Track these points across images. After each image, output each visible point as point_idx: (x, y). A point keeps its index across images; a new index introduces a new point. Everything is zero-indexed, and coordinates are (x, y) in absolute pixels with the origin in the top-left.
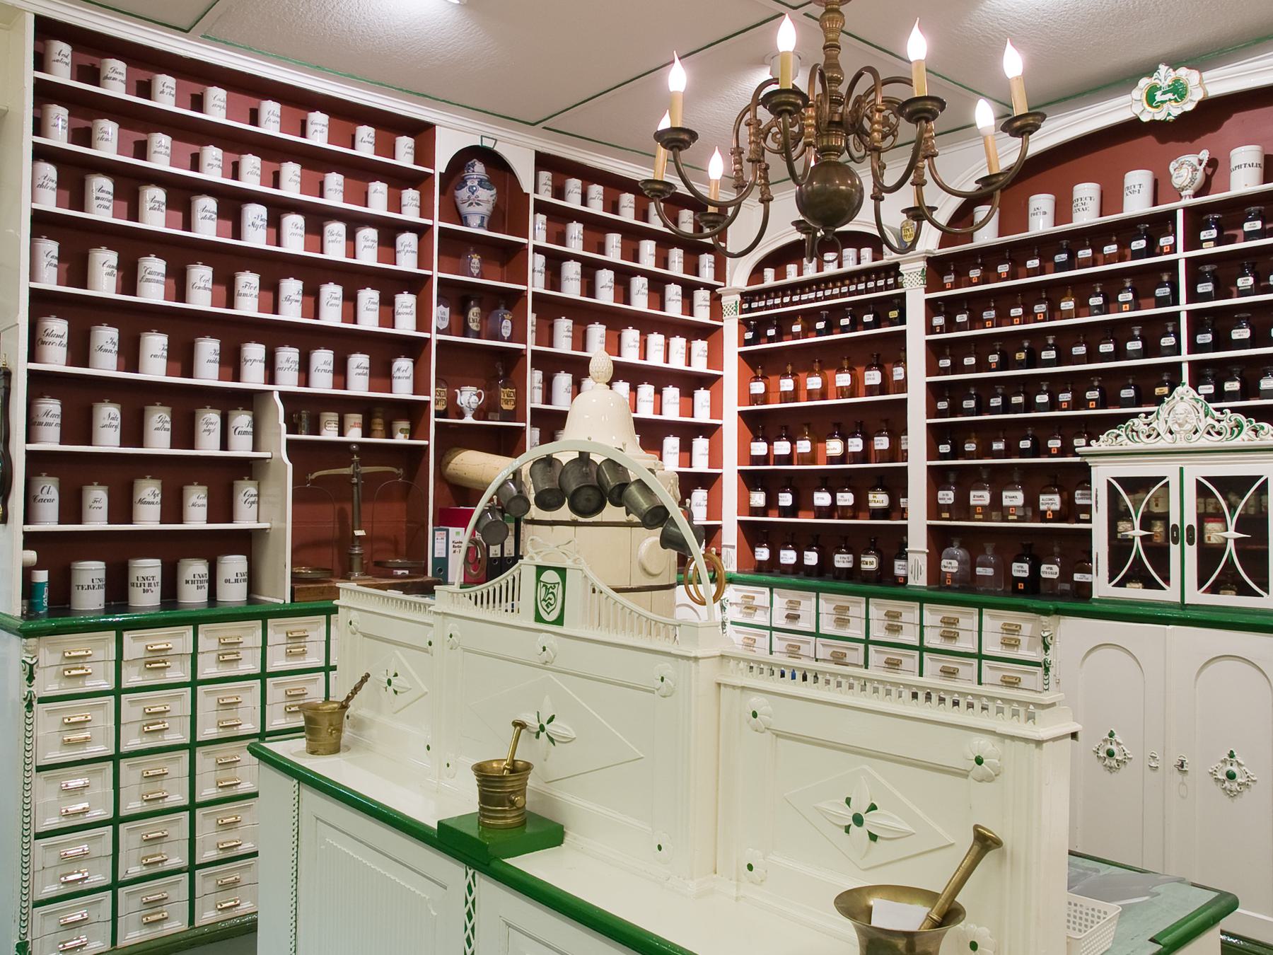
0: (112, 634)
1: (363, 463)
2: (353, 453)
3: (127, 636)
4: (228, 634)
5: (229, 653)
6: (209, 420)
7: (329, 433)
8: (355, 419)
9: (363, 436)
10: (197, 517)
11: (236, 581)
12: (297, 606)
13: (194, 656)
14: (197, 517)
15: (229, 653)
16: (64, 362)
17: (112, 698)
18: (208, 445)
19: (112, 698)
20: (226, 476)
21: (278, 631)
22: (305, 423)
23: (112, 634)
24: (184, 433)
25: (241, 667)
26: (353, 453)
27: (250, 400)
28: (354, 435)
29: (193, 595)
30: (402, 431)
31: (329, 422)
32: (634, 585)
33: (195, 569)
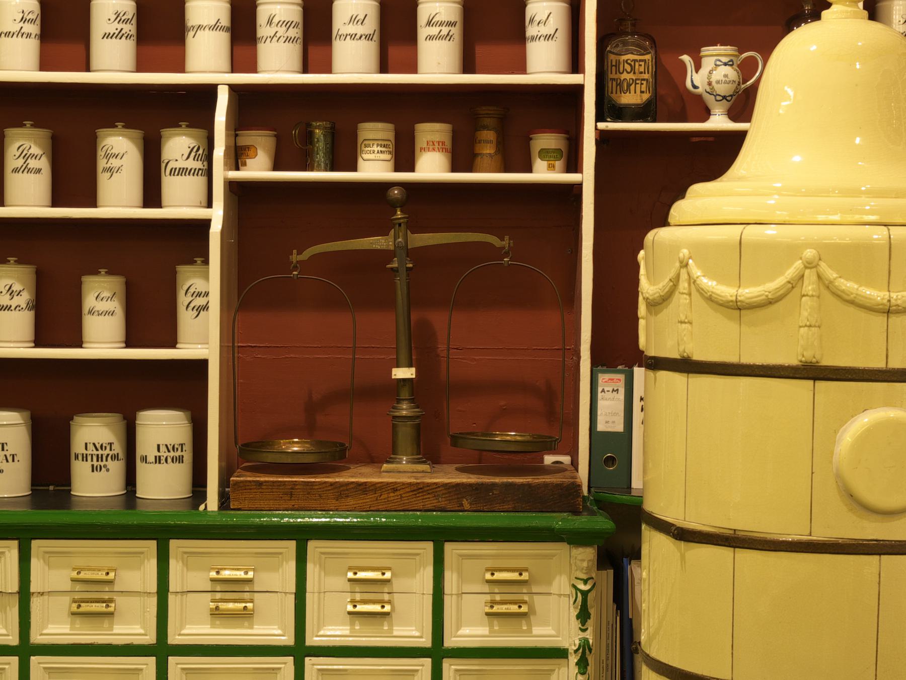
0: (427, 548)
1: (415, 226)
2: (393, 205)
3: (313, 547)
4: (94, 562)
5: (95, 599)
6: (119, 149)
7: (374, 167)
8: (432, 134)
9: (454, 169)
10: (103, 336)
11: (158, 460)
12: (234, 518)
13: (24, 595)
14: (103, 336)
15: (95, 599)
16: (225, 63)
17: (428, 662)
18: (118, 198)
19: (428, 662)
20: (153, 253)
21: (196, 568)
22: (488, 149)
23: (151, 546)
24: (74, 177)
25: (117, 629)
26: (393, 205)
27: (194, 104)
28: (432, 167)
29: (94, 483)
30: (544, 154)
31: (368, 142)
32: (820, 534)
33: (93, 432)
